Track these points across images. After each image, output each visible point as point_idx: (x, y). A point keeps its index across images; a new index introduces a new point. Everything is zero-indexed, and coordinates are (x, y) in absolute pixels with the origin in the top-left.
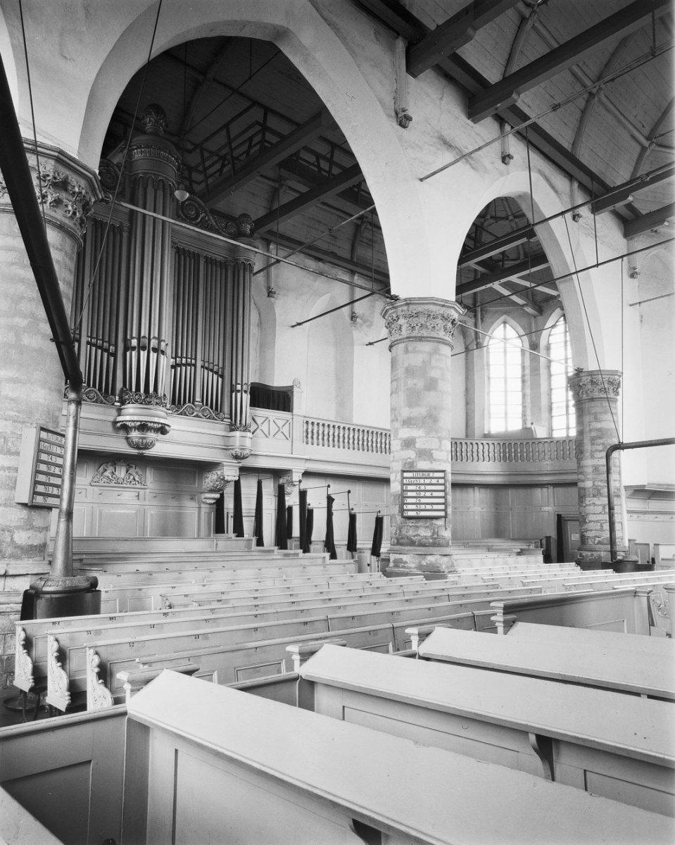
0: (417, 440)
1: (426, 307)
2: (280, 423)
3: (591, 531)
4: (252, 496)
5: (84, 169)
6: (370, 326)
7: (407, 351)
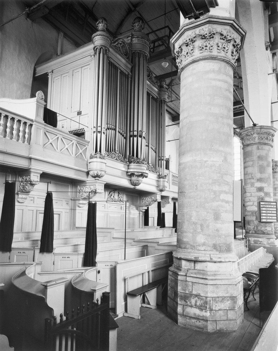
0: (265, 188)
1: (268, 130)
4: (55, 199)
7: (258, 149)
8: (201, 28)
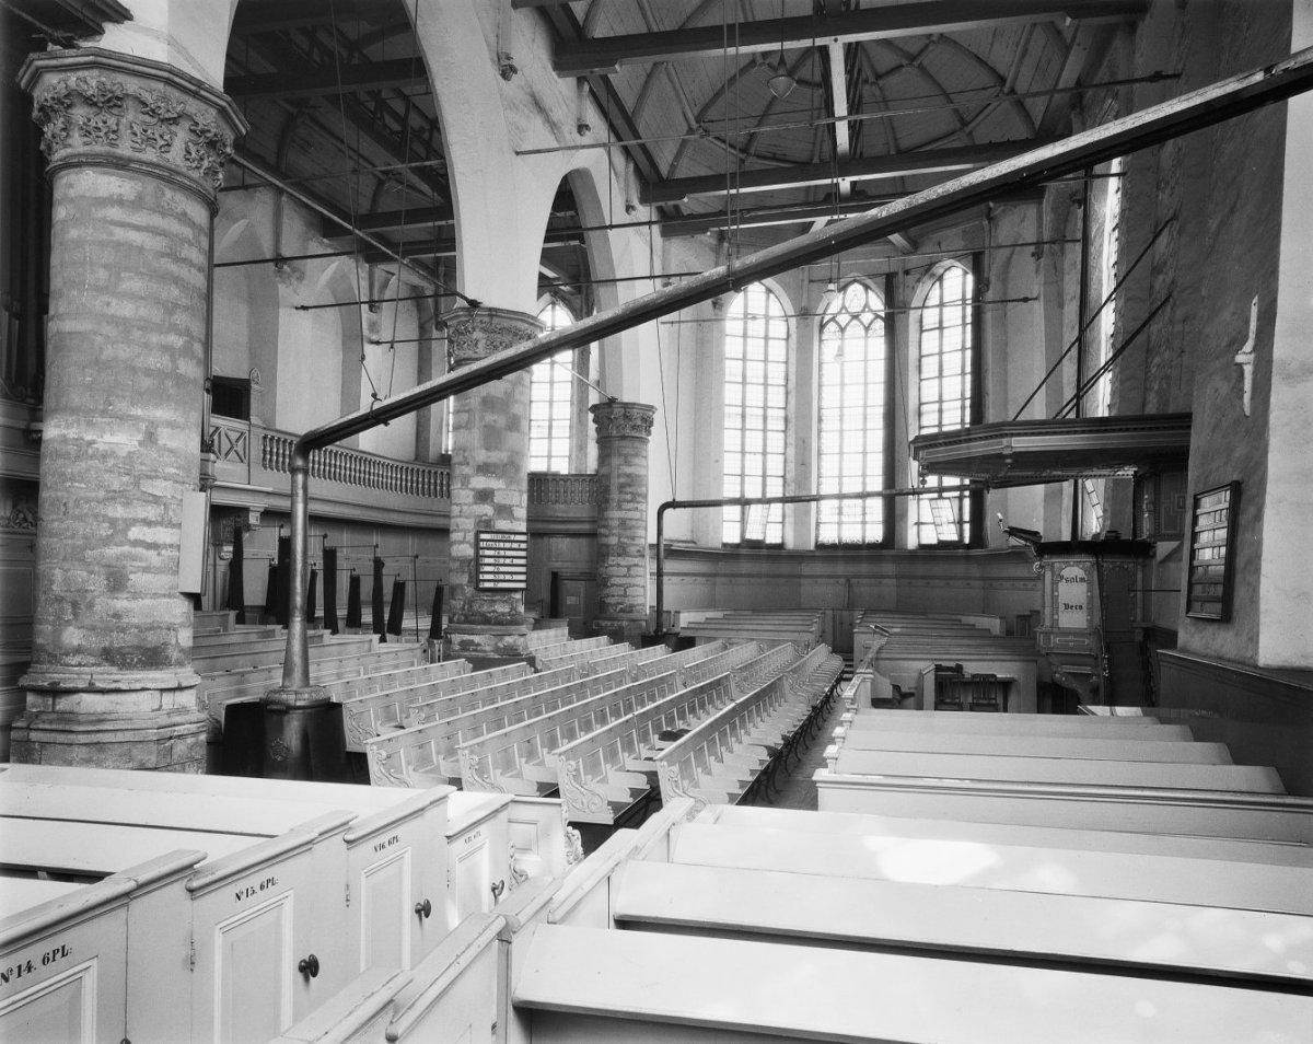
1: (514, 323)
2: (234, 436)
3: (613, 596)
5: (185, 88)
6: (301, 279)
8: (80, 74)
